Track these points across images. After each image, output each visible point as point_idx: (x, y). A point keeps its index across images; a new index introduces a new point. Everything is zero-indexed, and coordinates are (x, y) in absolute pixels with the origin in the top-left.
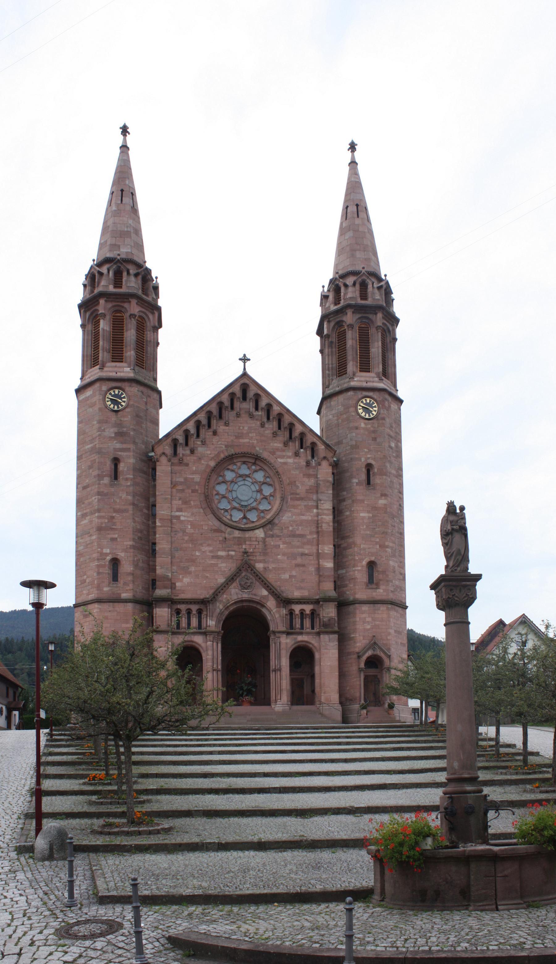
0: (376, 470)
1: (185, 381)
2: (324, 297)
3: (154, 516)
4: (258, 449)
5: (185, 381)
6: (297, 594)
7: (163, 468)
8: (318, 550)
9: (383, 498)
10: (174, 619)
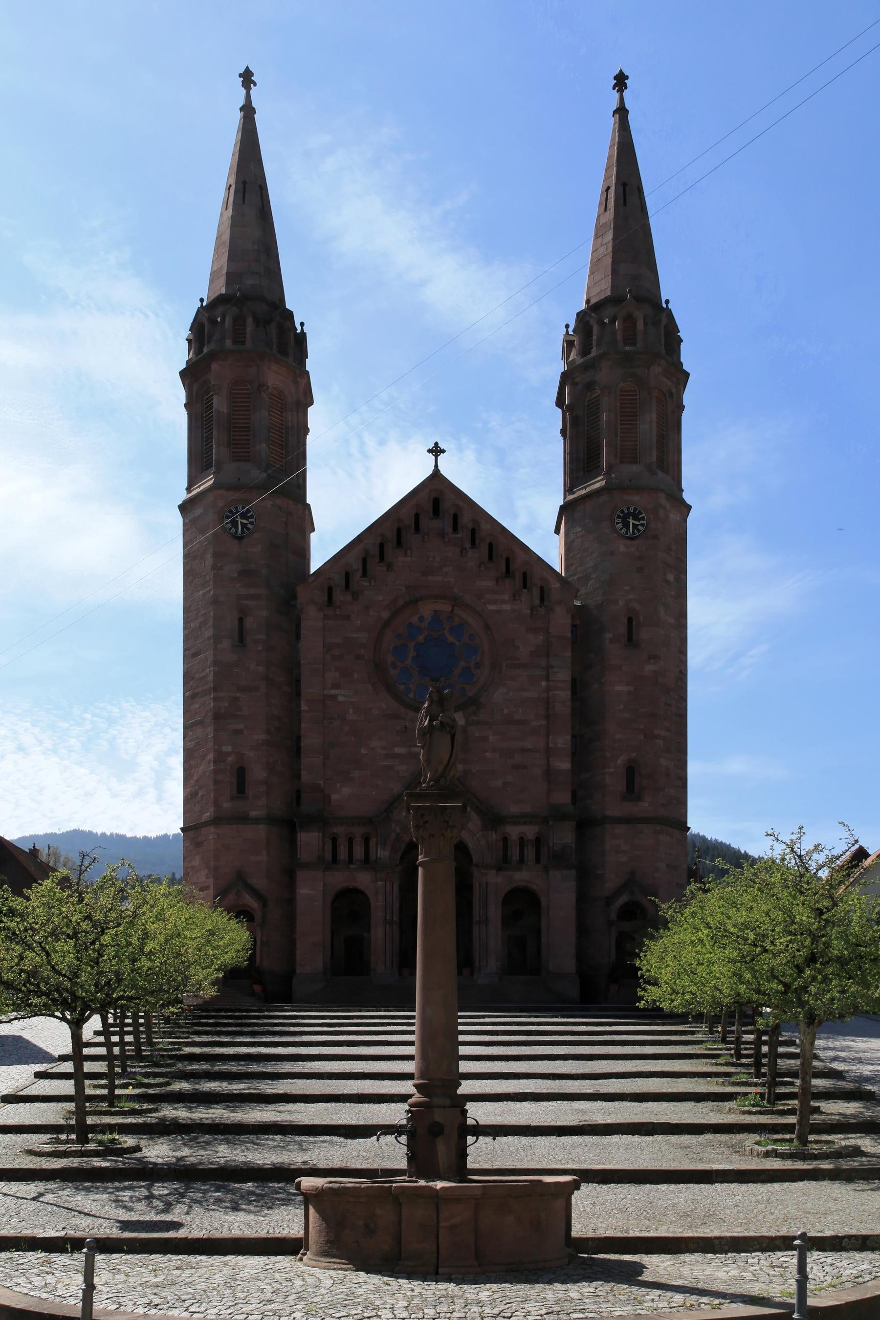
0: (641, 619)
1: (348, 492)
2: (569, 344)
3: (298, 694)
4: (456, 590)
5: (348, 492)
6: (514, 809)
7: (312, 620)
8: (548, 744)
9: (652, 661)
10: (329, 847)
